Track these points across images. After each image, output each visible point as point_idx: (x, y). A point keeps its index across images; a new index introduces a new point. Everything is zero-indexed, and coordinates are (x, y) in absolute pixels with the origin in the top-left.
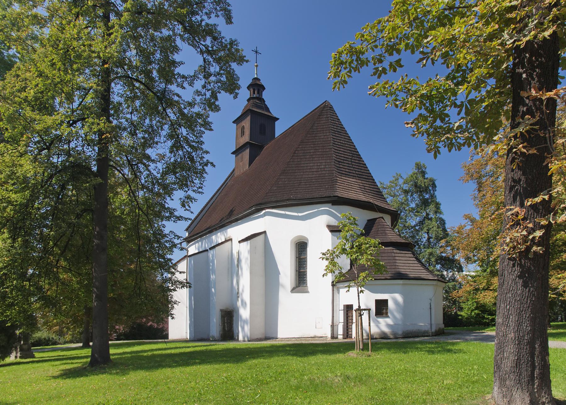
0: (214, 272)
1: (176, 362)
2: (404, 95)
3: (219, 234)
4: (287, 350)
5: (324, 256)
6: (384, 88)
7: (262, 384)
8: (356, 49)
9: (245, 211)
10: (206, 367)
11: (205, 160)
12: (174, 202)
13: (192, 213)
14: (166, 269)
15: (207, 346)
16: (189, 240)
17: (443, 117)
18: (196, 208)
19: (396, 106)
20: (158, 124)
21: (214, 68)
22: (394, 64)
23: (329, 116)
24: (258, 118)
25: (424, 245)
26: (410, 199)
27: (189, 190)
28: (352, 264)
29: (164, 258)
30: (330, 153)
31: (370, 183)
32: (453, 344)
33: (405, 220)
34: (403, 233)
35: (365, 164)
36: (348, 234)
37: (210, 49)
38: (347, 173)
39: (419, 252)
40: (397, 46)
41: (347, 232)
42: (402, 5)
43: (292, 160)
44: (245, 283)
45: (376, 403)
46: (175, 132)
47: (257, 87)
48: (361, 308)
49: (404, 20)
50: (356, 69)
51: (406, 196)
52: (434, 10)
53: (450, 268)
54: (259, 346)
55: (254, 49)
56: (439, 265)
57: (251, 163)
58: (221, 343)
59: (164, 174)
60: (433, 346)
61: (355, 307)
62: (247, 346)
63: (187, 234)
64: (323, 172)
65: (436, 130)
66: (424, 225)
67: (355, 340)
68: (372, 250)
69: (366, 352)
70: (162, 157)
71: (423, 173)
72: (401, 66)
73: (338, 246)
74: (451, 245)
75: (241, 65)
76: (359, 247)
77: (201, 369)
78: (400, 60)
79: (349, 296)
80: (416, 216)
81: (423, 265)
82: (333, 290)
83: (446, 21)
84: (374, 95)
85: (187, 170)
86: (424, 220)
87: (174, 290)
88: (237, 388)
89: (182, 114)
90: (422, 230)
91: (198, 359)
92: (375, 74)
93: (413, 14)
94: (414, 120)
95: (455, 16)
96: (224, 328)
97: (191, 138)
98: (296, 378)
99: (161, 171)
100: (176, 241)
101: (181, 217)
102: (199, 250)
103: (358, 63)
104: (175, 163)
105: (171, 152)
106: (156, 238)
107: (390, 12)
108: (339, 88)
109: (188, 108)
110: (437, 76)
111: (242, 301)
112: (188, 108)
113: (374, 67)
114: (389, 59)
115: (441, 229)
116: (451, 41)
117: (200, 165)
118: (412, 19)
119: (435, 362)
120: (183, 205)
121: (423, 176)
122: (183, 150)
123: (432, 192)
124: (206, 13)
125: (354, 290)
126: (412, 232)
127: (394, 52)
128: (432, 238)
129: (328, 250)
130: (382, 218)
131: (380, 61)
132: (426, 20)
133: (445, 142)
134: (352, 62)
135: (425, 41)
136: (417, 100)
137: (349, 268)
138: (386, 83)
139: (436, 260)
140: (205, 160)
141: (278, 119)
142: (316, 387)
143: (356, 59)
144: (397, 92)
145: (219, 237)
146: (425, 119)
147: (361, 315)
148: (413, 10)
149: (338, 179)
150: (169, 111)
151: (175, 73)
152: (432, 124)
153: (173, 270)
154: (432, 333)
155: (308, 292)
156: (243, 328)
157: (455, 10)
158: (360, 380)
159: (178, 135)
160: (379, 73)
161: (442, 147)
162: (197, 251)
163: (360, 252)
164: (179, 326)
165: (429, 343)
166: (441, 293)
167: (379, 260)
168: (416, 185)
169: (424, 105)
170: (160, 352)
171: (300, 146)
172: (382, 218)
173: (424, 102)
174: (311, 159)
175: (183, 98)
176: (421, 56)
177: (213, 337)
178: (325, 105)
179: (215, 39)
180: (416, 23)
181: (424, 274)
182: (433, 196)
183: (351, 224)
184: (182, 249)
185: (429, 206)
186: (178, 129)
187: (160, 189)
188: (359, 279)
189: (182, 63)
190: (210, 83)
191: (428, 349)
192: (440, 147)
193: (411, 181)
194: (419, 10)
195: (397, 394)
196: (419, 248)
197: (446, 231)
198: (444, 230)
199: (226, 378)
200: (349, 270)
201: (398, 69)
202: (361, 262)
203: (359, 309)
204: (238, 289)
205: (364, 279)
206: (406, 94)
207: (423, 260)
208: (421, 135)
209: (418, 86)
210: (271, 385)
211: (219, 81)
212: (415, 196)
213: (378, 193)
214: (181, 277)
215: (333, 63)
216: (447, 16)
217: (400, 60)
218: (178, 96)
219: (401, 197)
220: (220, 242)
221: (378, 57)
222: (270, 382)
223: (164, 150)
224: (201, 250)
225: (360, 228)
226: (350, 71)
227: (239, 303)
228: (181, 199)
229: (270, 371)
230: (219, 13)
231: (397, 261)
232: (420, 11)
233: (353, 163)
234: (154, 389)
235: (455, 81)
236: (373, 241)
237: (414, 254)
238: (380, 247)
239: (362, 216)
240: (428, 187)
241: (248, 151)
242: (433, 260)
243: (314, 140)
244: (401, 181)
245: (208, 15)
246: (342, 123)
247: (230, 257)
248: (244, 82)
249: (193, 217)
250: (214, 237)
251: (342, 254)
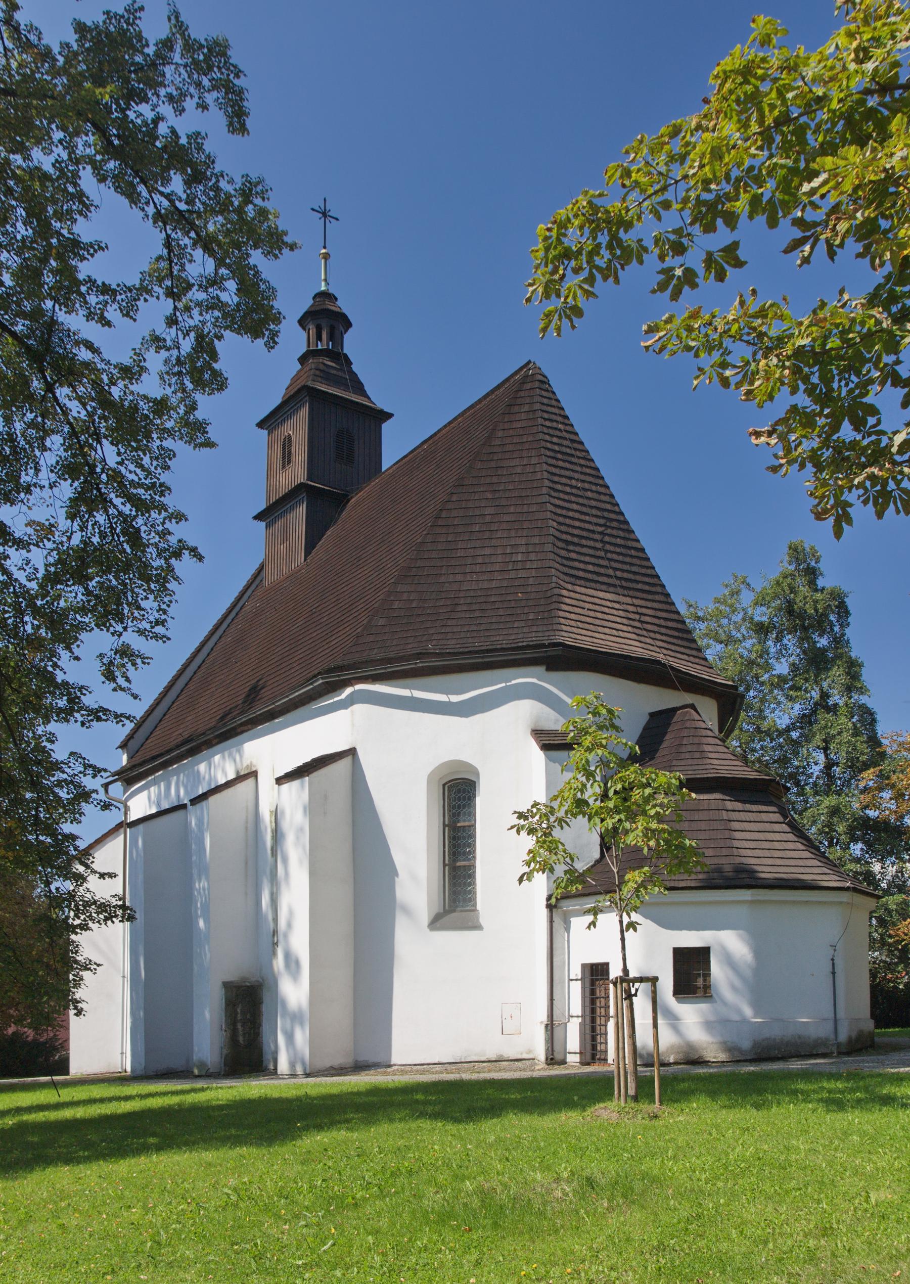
0: (204, 870)
1: (88, 1146)
2: (746, 351)
3: (217, 758)
4: (417, 1102)
5: (522, 822)
6: (690, 329)
7: (342, 1207)
8: (607, 212)
9: (294, 689)
10: (177, 1158)
11: (173, 540)
12: (80, 664)
13: (135, 697)
14: (59, 868)
15: (182, 1092)
16: (129, 777)
17: (861, 414)
18: (149, 683)
19: (725, 382)
20: (32, 432)
21: (200, 265)
22: (717, 256)
23: (537, 406)
24: (334, 415)
25: (815, 784)
26: (772, 650)
27: (125, 629)
28: (605, 847)
29: (53, 834)
30: (541, 516)
31: (655, 605)
32: (899, 1079)
33: (761, 711)
34: (754, 750)
35: (642, 550)
36: (591, 757)
37: (182, 206)
38: (590, 576)
39: (799, 807)
40: (728, 205)
41: (589, 750)
42: (740, 79)
43: (429, 538)
44: (295, 899)
45: (672, 1261)
46: (84, 455)
47: (326, 318)
48: (632, 974)
49: (746, 126)
50: (608, 273)
51: (762, 642)
52: (836, 95)
53: (890, 854)
54: (335, 1091)
55: (318, 204)
56: (860, 845)
57: (310, 546)
58: (226, 1083)
59: (52, 579)
60: (840, 1085)
61: (615, 972)
62: (300, 1092)
63: (125, 758)
64: (522, 574)
65: (840, 453)
66: (815, 727)
67: (613, 1068)
68: (661, 805)
69: (645, 1107)
70: (46, 530)
71: (812, 574)
72: (739, 264)
73: (562, 791)
74: (893, 786)
75: (276, 257)
76: (625, 794)
77: (161, 1167)
78: (735, 245)
79: (596, 938)
80: (790, 699)
81: (810, 844)
82: (551, 921)
83: (870, 126)
84: (662, 350)
85: (116, 568)
86: (814, 712)
87: (84, 927)
88: (268, 1222)
89: (104, 400)
90: (808, 741)
91: (154, 1135)
92: (662, 287)
93: (772, 107)
94: (777, 423)
95: (894, 112)
96: (233, 1040)
97: (131, 473)
98: (440, 1188)
99: (40, 575)
100: (89, 783)
101: (105, 711)
102: (158, 804)
103: (613, 255)
104: (84, 550)
105: (71, 517)
106: (29, 773)
107: (706, 101)
108: (559, 330)
109: (121, 384)
110: (842, 292)
111: (288, 956)
112: (121, 384)
113: (660, 266)
114: (704, 243)
115: (865, 738)
116: (883, 190)
117: (159, 555)
118: (769, 121)
119: (846, 1134)
120: (109, 675)
121: (812, 583)
122: (106, 512)
123: (836, 629)
124: (170, 98)
125: (609, 921)
126: (781, 746)
127: (719, 222)
128: (837, 764)
129: (536, 804)
130: (692, 706)
131: (679, 249)
132: (813, 125)
133: (866, 489)
134: (596, 251)
135: (806, 187)
136: (784, 367)
137: (597, 855)
138: (694, 316)
139: (851, 830)
140: (173, 540)
141: (389, 416)
142: (499, 1215)
143: (609, 245)
144: (727, 342)
145: (219, 766)
146: (808, 421)
147: (630, 997)
148: (774, 95)
149: (564, 592)
150: (62, 392)
151: (81, 276)
152: (828, 439)
153: (81, 869)
154: (839, 1045)
155: (478, 927)
156: (290, 1038)
157: (897, 94)
158: (626, 1191)
159: (92, 467)
160: (675, 285)
161: (858, 504)
162: (154, 810)
163: (628, 810)
164: (101, 1034)
165: (832, 1076)
166: (863, 925)
167: (680, 834)
168: (790, 610)
169: (806, 379)
170: (40, 1117)
171: (454, 498)
172: (692, 706)
173: (806, 369)
174: (487, 535)
175: (105, 356)
176: (798, 234)
177: (202, 1065)
178: (527, 376)
179: (195, 177)
180: (783, 134)
181: (811, 869)
182: (839, 641)
183: (601, 728)
184: (106, 806)
185: (829, 669)
186: (91, 446)
187: (39, 627)
188: (625, 890)
189: (98, 247)
190: (188, 309)
191: (825, 1095)
192: (851, 505)
193: (776, 597)
194: (790, 95)
195: (734, 1234)
196: (801, 793)
197: (879, 744)
198: (874, 741)
199: (235, 1190)
200: (598, 862)
201: (730, 271)
202: (630, 839)
203: (625, 978)
204: (275, 920)
205: (637, 890)
206: (751, 349)
207: (814, 830)
208: (796, 466)
209: (786, 325)
210: (368, 1210)
211: (215, 304)
212: (789, 640)
213: (682, 636)
214: (101, 890)
215: (541, 254)
216: (872, 111)
217: (735, 245)
218: (89, 346)
219: (748, 643)
220: (222, 781)
221: (672, 237)
222: (364, 1199)
223: (51, 511)
224: (166, 805)
225: (627, 740)
226: (591, 280)
227: (279, 962)
228: (101, 656)
229: (364, 1167)
230: (210, 98)
231: (738, 835)
232: (795, 98)
233: (608, 547)
234: (18, 1233)
235: (894, 309)
236: (663, 778)
237: (784, 813)
238: (683, 795)
239: (635, 702)
240: (827, 616)
241: (301, 511)
242: (841, 828)
243: (495, 480)
244: (747, 598)
245: (176, 101)
246: (577, 428)
247: (251, 825)
248: (291, 303)
249: (138, 710)
250: (202, 767)
251: (575, 815)
